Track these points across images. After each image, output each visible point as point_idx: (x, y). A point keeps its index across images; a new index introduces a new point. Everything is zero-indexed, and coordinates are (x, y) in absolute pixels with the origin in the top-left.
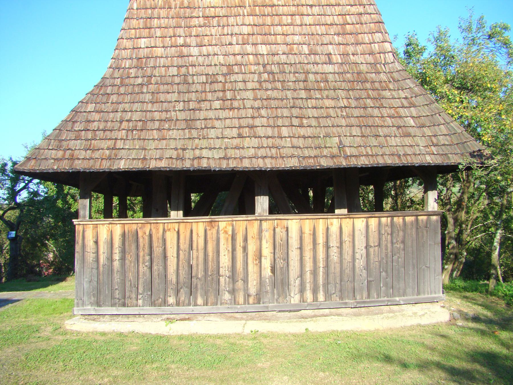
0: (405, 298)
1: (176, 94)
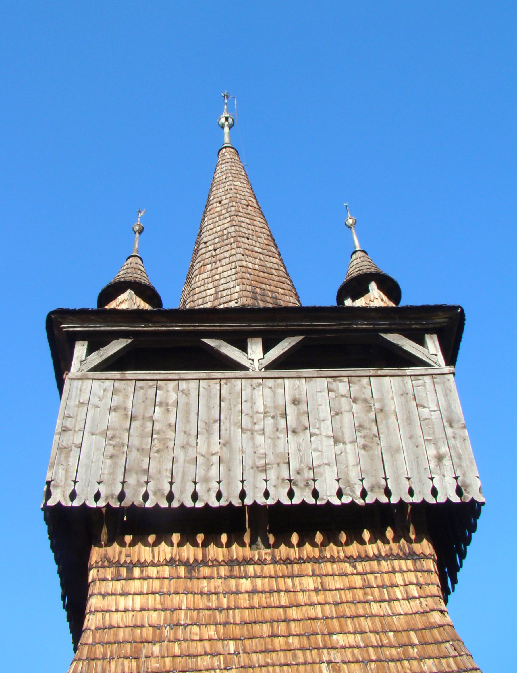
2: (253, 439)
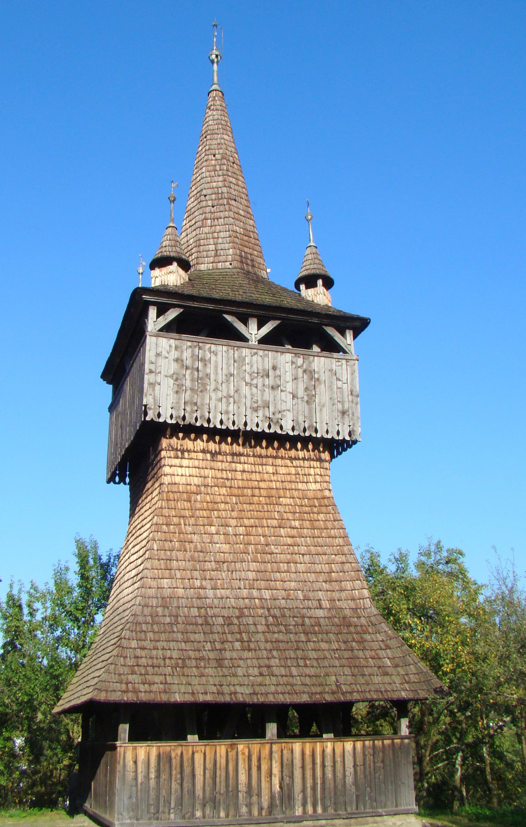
0: (386, 809)
1: (202, 634)
2: (251, 389)
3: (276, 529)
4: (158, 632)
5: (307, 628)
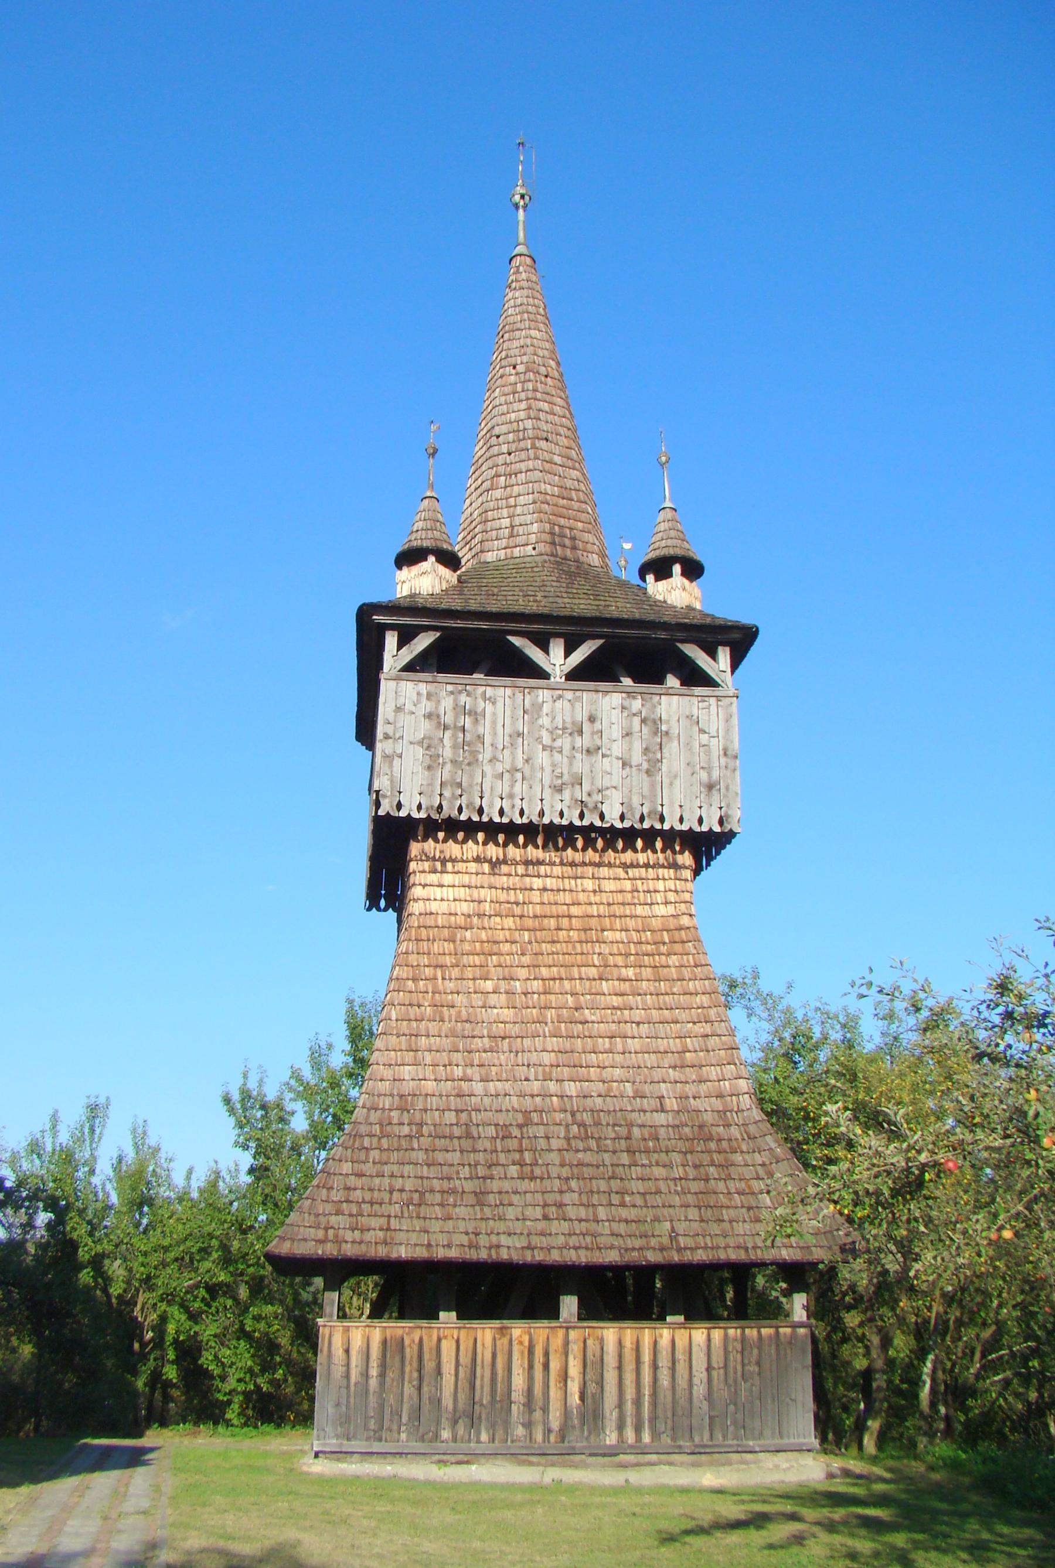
0: (762, 1442)
1: (458, 1153)
2: (552, 756)
3: (594, 983)
4: (388, 1150)
5: (634, 1143)
